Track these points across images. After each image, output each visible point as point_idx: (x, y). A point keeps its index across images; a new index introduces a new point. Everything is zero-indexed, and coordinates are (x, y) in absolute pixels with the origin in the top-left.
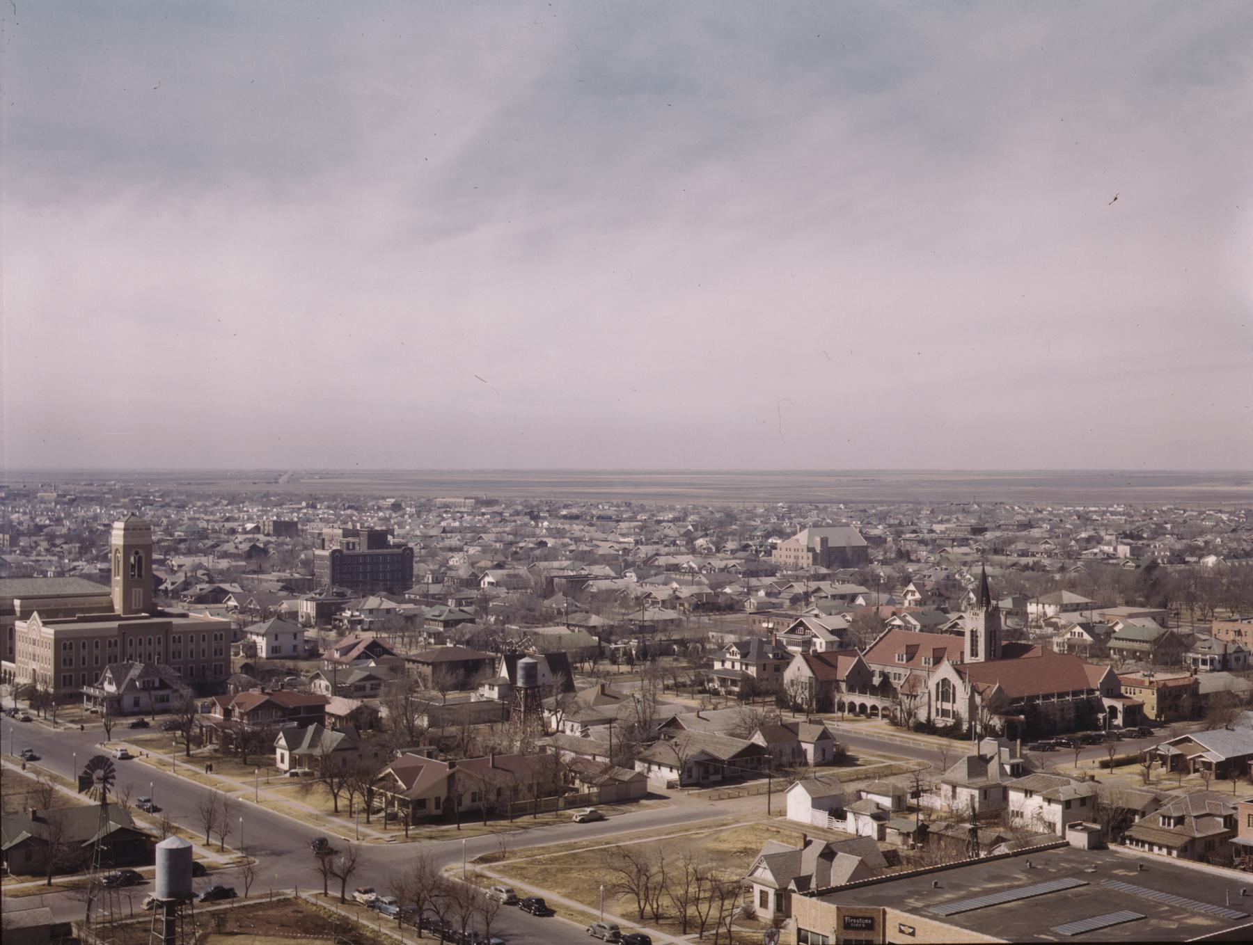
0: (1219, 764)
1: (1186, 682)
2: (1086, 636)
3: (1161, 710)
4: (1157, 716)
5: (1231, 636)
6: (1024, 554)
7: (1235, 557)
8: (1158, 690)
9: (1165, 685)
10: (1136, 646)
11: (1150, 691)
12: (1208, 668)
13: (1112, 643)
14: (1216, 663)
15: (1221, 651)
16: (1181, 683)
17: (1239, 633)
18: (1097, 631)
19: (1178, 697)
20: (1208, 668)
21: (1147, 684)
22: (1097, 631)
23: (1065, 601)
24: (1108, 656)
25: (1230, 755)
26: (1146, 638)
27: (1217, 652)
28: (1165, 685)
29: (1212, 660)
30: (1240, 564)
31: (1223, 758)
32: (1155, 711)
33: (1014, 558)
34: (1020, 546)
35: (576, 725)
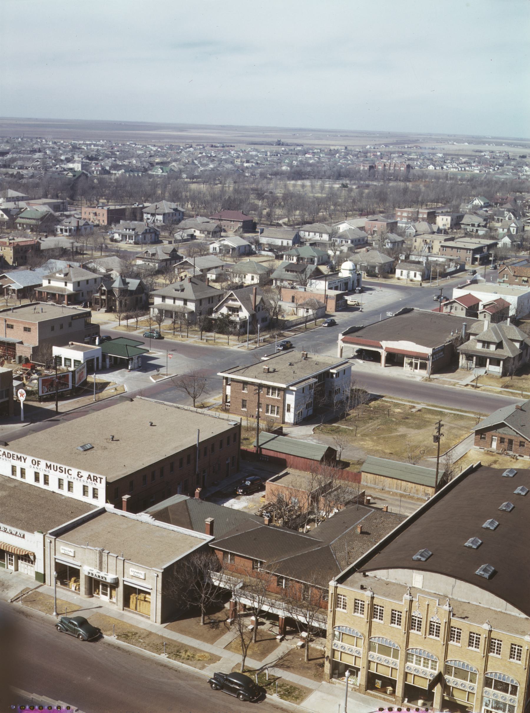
0: (19, 291)
1: (32, 243)
2: (5, 217)
3: (15, 259)
4: (14, 262)
5: (92, 216)
6: (21, 167)
7: (131, 171)
8: (14, 248)
9: (18, 245)
10: (28, 221)
11: (10, 248)
12: (68, 234)
13: (19, 220)
14: (73, 231)
15: (76, 225)
16: (29, 243)
17: (95, 214)
18: (12, 213)
19: (26, 251)
20: (68, 234)
21: (8, 244)
22: (12, 213)
23: (9, 196)
24: (16, 228)
25: (26, 285)
26: (34, 217)
27: (74, 225)
28: (18, 245)
29: (70, 230)
30: (134, 175)
31: (22, 287)
32: (12, 260)
33: (15, 171)
34: (20, 163)
35: (255, 276)
